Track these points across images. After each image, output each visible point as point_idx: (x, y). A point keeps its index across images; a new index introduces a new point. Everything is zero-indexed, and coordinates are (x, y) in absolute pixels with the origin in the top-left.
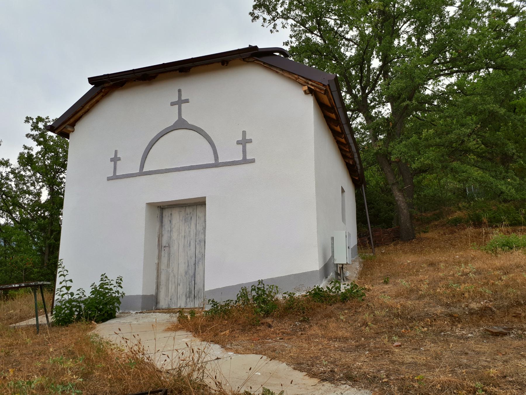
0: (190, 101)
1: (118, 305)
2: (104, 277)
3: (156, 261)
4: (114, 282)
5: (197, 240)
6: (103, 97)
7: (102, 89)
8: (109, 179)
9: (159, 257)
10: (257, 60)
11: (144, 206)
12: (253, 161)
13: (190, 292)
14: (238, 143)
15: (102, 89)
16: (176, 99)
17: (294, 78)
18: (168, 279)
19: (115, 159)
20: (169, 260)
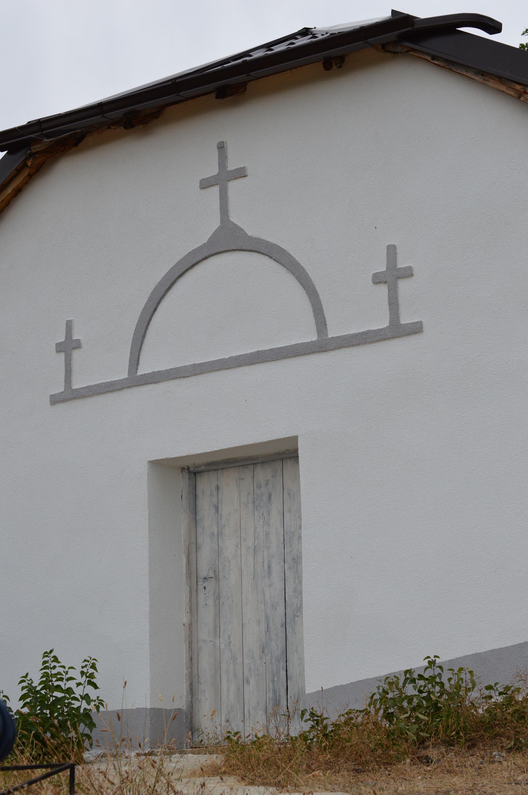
0: (249, 172)
1: (87, 731)
2: (50, 658)
3: (185, 620)
4: (75, 674)
5: (288, 558)
6: (31, 178)
7: (27, 159)
8: (55, 400)
9: (193, 608)
10: (413, 50)
11: (144, 469)
12: (416, 329)
13: (277, 703)
14: (377, 279)
15: (27, 159)
16: (213, 170)
17: (513, 93)
18: (217, 668)
19: (68, 347)
20: (218, 615)
